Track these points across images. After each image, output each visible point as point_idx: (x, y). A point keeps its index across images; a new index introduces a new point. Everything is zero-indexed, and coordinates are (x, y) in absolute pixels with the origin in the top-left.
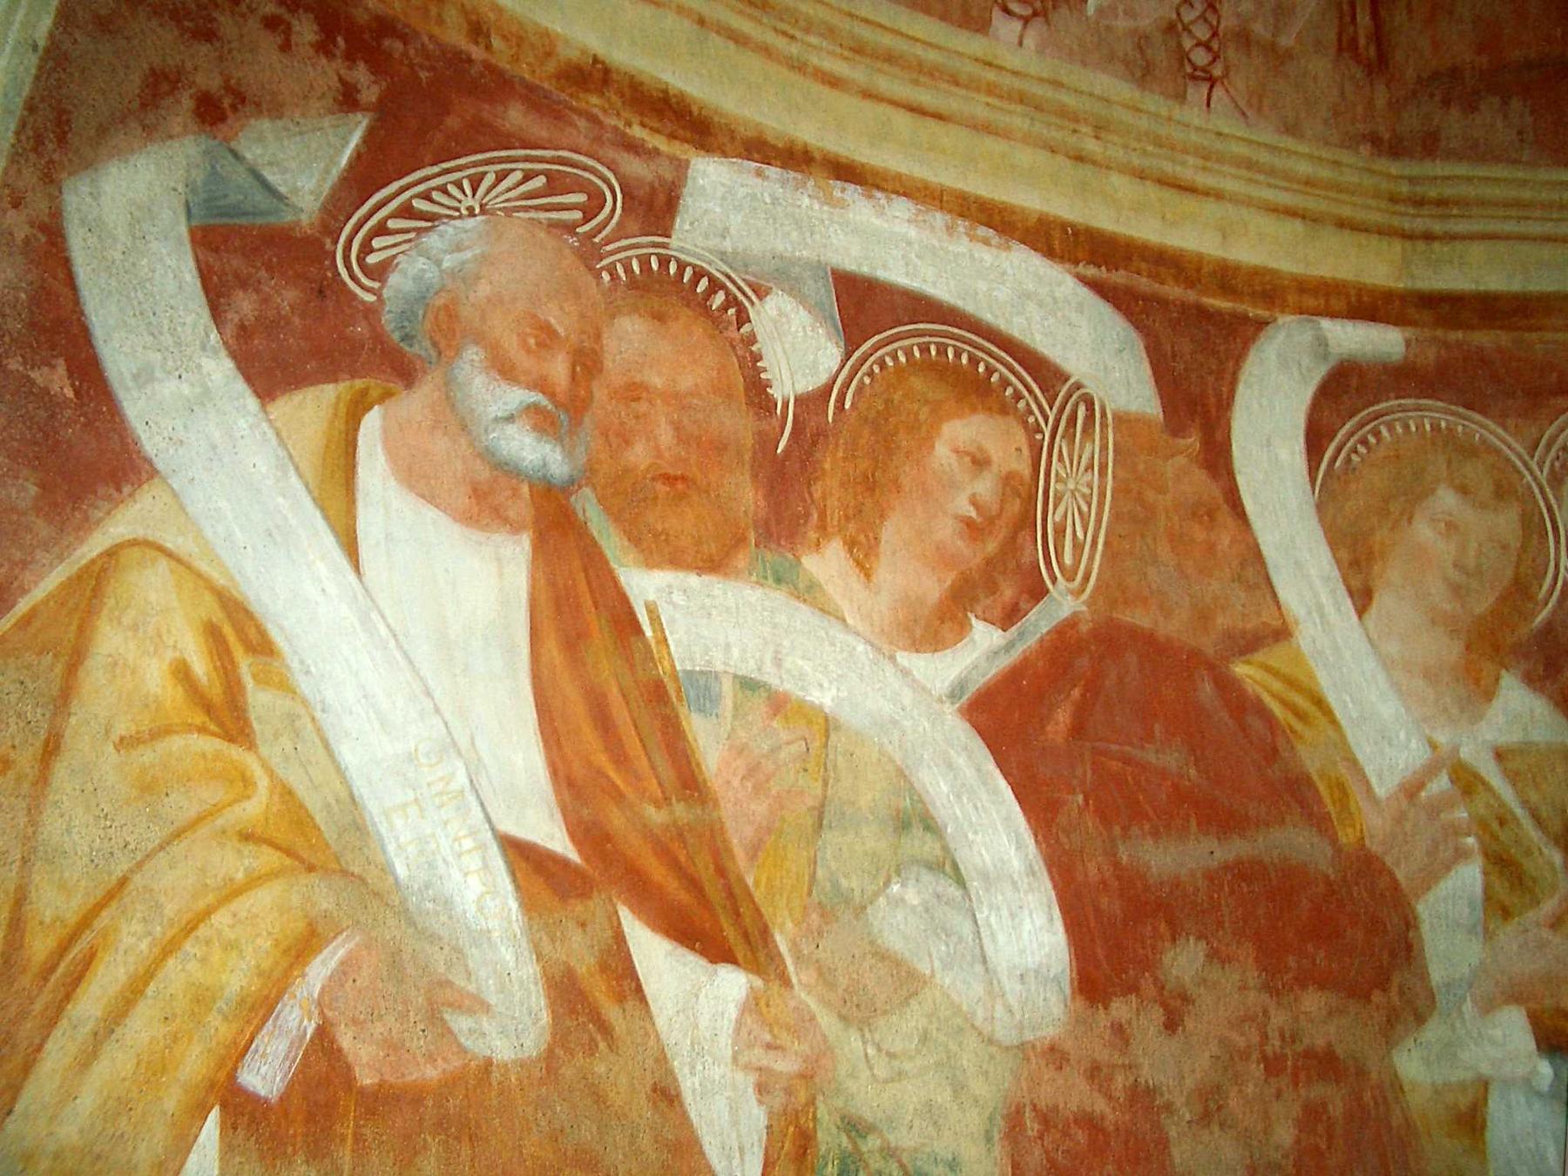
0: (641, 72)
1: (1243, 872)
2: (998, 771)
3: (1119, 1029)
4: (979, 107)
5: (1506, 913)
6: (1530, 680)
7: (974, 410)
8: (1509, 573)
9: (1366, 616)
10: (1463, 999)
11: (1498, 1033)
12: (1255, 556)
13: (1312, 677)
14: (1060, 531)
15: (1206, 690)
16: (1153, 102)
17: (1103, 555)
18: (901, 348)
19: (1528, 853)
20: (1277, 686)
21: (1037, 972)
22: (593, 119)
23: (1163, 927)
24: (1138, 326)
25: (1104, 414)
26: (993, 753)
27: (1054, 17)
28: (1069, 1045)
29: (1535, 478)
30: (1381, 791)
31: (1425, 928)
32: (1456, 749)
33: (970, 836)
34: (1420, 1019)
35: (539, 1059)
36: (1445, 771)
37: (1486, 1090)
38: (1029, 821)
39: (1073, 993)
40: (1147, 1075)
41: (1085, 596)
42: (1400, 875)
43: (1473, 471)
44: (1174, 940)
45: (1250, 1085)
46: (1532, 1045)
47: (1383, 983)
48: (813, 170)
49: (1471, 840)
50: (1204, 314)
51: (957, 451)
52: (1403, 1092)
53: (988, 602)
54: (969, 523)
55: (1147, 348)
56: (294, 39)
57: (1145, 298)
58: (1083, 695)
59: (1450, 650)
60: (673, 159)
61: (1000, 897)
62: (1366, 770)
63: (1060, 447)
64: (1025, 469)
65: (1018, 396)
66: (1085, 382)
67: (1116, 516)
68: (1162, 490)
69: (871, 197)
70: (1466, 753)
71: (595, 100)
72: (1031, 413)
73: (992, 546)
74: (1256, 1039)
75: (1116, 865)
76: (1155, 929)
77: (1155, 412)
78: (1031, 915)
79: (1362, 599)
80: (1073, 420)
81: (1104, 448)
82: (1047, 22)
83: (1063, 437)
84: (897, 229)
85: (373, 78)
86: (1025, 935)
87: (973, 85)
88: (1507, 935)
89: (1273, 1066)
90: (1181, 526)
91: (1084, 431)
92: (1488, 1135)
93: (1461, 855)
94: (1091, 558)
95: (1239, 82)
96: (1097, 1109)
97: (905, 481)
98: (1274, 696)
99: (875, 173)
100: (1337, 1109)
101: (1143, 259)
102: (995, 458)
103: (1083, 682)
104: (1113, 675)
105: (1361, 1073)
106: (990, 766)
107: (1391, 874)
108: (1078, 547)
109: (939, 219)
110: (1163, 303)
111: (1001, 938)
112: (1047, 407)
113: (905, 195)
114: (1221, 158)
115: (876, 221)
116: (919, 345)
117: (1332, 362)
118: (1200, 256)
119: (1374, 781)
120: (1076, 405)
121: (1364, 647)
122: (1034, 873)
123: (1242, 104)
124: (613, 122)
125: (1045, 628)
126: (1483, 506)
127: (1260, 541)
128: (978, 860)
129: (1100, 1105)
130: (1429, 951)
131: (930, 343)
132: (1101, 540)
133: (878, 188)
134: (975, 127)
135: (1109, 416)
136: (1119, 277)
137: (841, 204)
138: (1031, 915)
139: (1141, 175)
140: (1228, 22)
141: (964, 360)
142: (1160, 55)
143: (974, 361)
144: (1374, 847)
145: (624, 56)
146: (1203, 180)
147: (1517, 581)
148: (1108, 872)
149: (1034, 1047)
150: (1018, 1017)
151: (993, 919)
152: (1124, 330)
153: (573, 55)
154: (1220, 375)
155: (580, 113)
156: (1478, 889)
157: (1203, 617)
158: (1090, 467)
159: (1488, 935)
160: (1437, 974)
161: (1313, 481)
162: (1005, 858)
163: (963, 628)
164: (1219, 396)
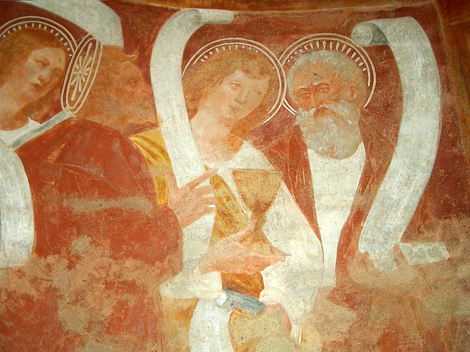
1: (111, 213)
2: (25, 172)
3: (48, 266)
5: (222, 234)
6: (255, 144)
7: (46, 46)
8: (259, 103)
9: (192, 120)
10: (195, 267)
11: (207, 282)
12: (152, 96)
13: (163, 142)
14: (72, 88)
15: (117, 145)
17: (87, 97)
18: (20, 25)
19: (237, 212)
20: (146, 144)
21: (20, 243)
23: (75, 231)
24: (119, 14)
25: (99, 46)
26: (24, 166)
28: (26, 271)
29: (279, 67)
30: (179, 185)
31: (185, 239)
32: (216, 170)
33: (7, 194)
34: (175, 273)
36: (209, 179)
37: (196, 303)
38: (31, 190)
39: (33, 252)
40: (55, 284)
41: (76, 112)
42: (179, 217)
43: (253, 65)
44: (78, 235)
45: (98, 292)
46: (221, 287)
47: (161, 258)
49: (213, 206)
51: (37, 61)
52: (161, 300)
53: (37, 113)
54: (36, 86)
55: (122, 22)
58: (66, 147)
59: (225, 132)
61: (12, 216)
62: (176, 177)
63: (79, 59)
64: (62, 66)
65: (65, 41)
66: (94, 35)
67: (96, 83)
68: (117, 73)
70: (219, 173)
72: (69, 47)
73: (43, 94)
74: (104, 276)
75: (61, 207)
76: (71, 231)
77: (121, 45)
78: (22, 222)
79: (192, 112)
80: (86, 49)
81: (97, 59)
83: (80, 55)
86: (18, 230)
88: (220, 243)
89: (109, 285)
90: (122, 87)
91: (90, 53)
92: (192, 320)
93: (207, 211)
94: (83, 98)
96: (32, 294)
97: (14, 71)
98: (145, 148)
100: (131, 304)
102: (51, 64)
103: (67, 142)
104: (80, 139)
105: (145, 292)
106: (22, 170)
107: (175, 218)
108: (78, 94)
111: (9, 230)
112: (76, 44)
116: (28, 24)
117: (201, 25)
119: (178, 182)
120: (89, 43)
121: (189, 131)
122: (28, 208)
125: (57, 122)
126: (255, 78)
127: (154, 92)
128: (8, 202)
129: (33, 293)
130: (185, 247)
131: (32, 23)
132: (88, 92)
135: (102, 47)
138: (22, 222)
141: (45, 28)
143: (49, 28)
144: (170, 206)
147: (261, 106)
148: (57, 209)
149: (12, 269)
150: (8, 258)
151: (7, 223)
154: (151, 31)
156: (211, 225)
157: (123, 118)
158: (89, 66)
159: (212, 243)
160: (186, 258)
161: (183, 69)
162: (19, 202)
163: (25, 122)
164: (149, 38)
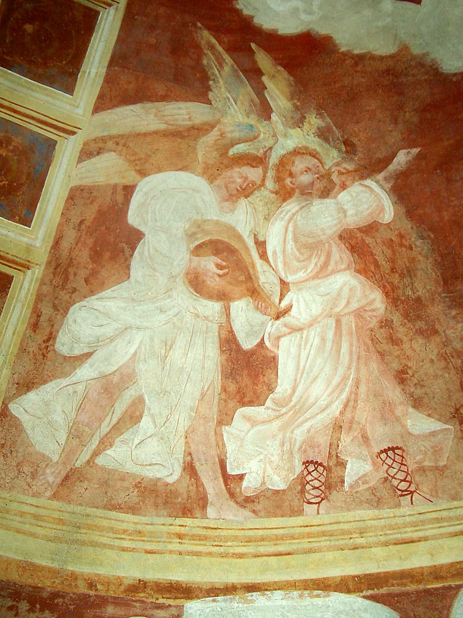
0: (159, 579)
4: (305, 544)
16: (386, 512)
22: (143, 602)
27: (331, 497)
35: (411, 54)
48: (237, 593)
50: (427, 592)
56: (20, 611)
57: (398, 595)
60: (176, 606)
69: (264, 595)
71: (142, 595)
82: (329, 501)
84: (277, 604)
85: (51, 615)
87: (302, 536)
95: (425, 488)
99: (264, 584)
101: (395, 579)
109: (296, 593)
110: (407, 594)
113: (279, 589)
114: (423, 522)
115: (269, 603)
118: (422, 568)
123: (428, 497)
124: (151, 600)
133: (267, 590)
134: (306, 553)
136: (384, 590)
137: (252, 601)
139: (386, 544)
140: (412, 465)
142: (385, 493)
145: (151, 576)
146: (416, 535)
152: (389, 613)
153: (131, 582)
155: (136, 601)
